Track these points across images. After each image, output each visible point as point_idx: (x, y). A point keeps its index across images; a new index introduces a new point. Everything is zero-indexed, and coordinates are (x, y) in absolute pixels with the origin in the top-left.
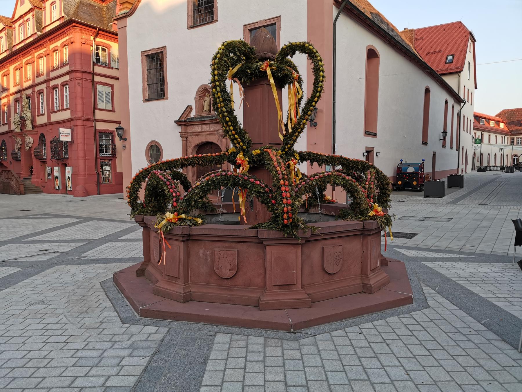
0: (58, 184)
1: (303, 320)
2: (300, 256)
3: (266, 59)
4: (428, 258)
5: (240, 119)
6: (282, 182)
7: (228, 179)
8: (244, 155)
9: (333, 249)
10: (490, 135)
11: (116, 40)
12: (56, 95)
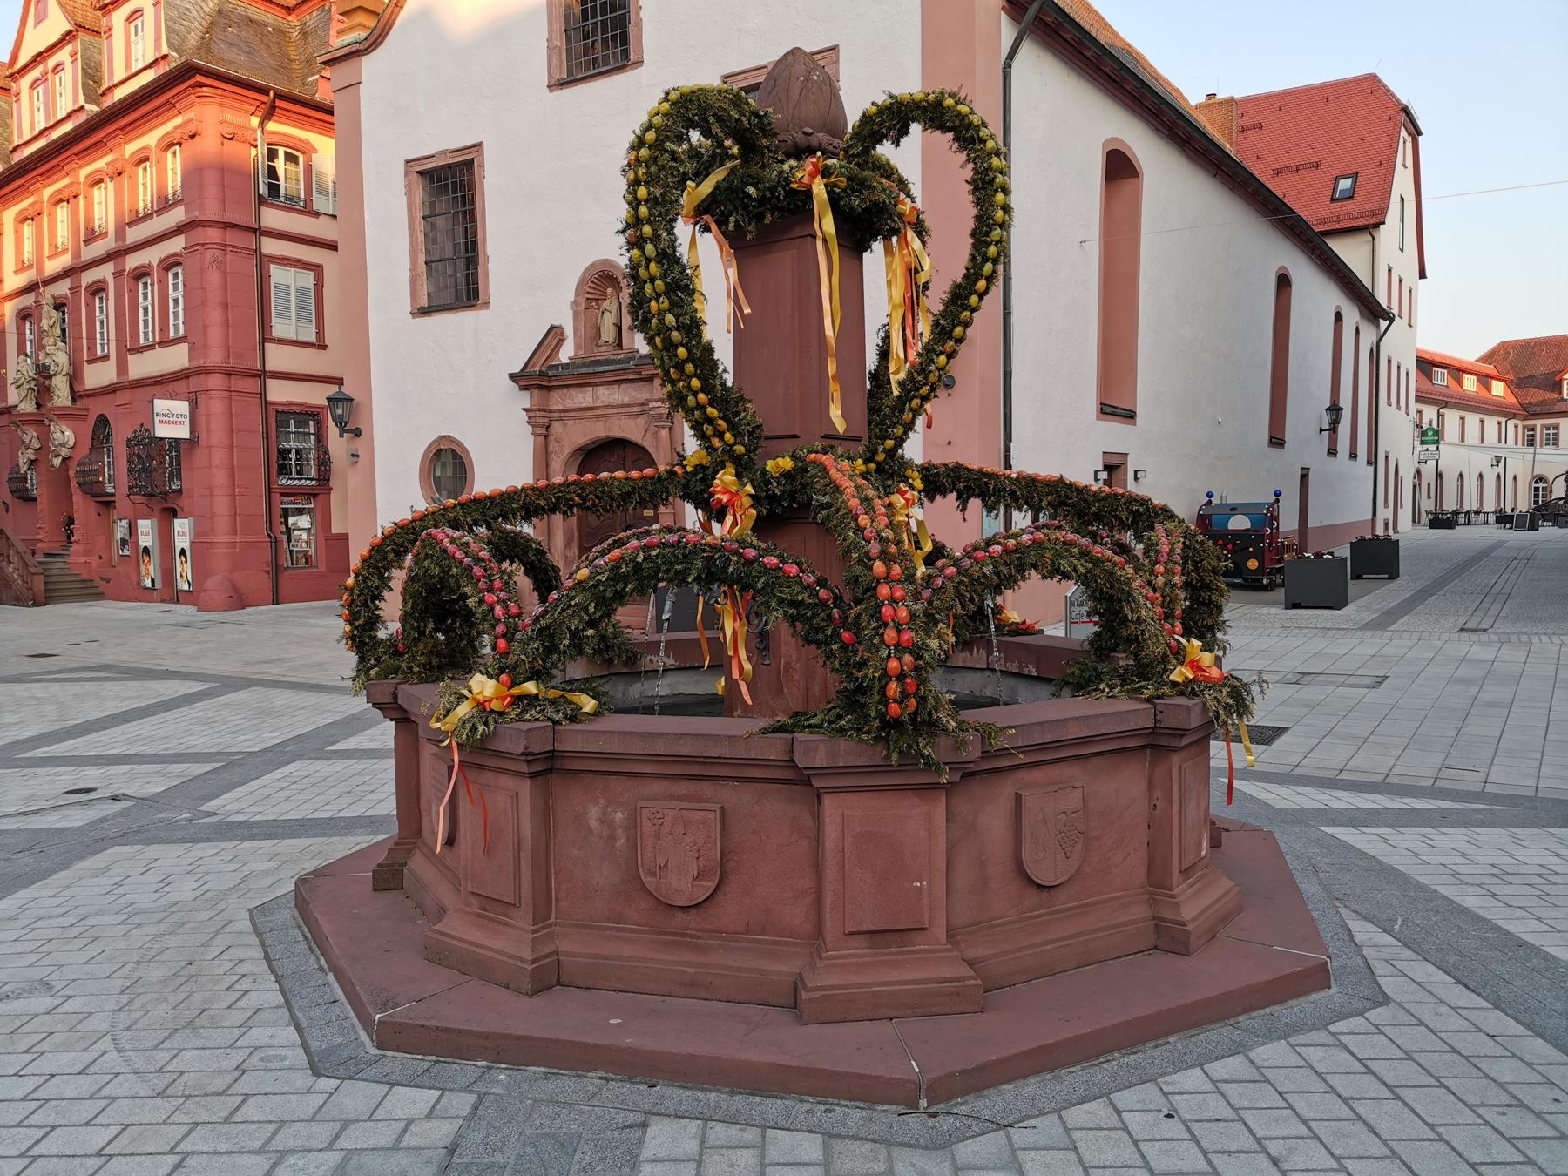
0: (150, 571)
1: (960, 1067)
2: (943, 825)
5: (724, 354)
6: (879, 567)
7: (687, 558)
8: (739, 476)
9: (1053, 798)
10: (1462, 419)
11: (327, 128)
12: (145, 298)
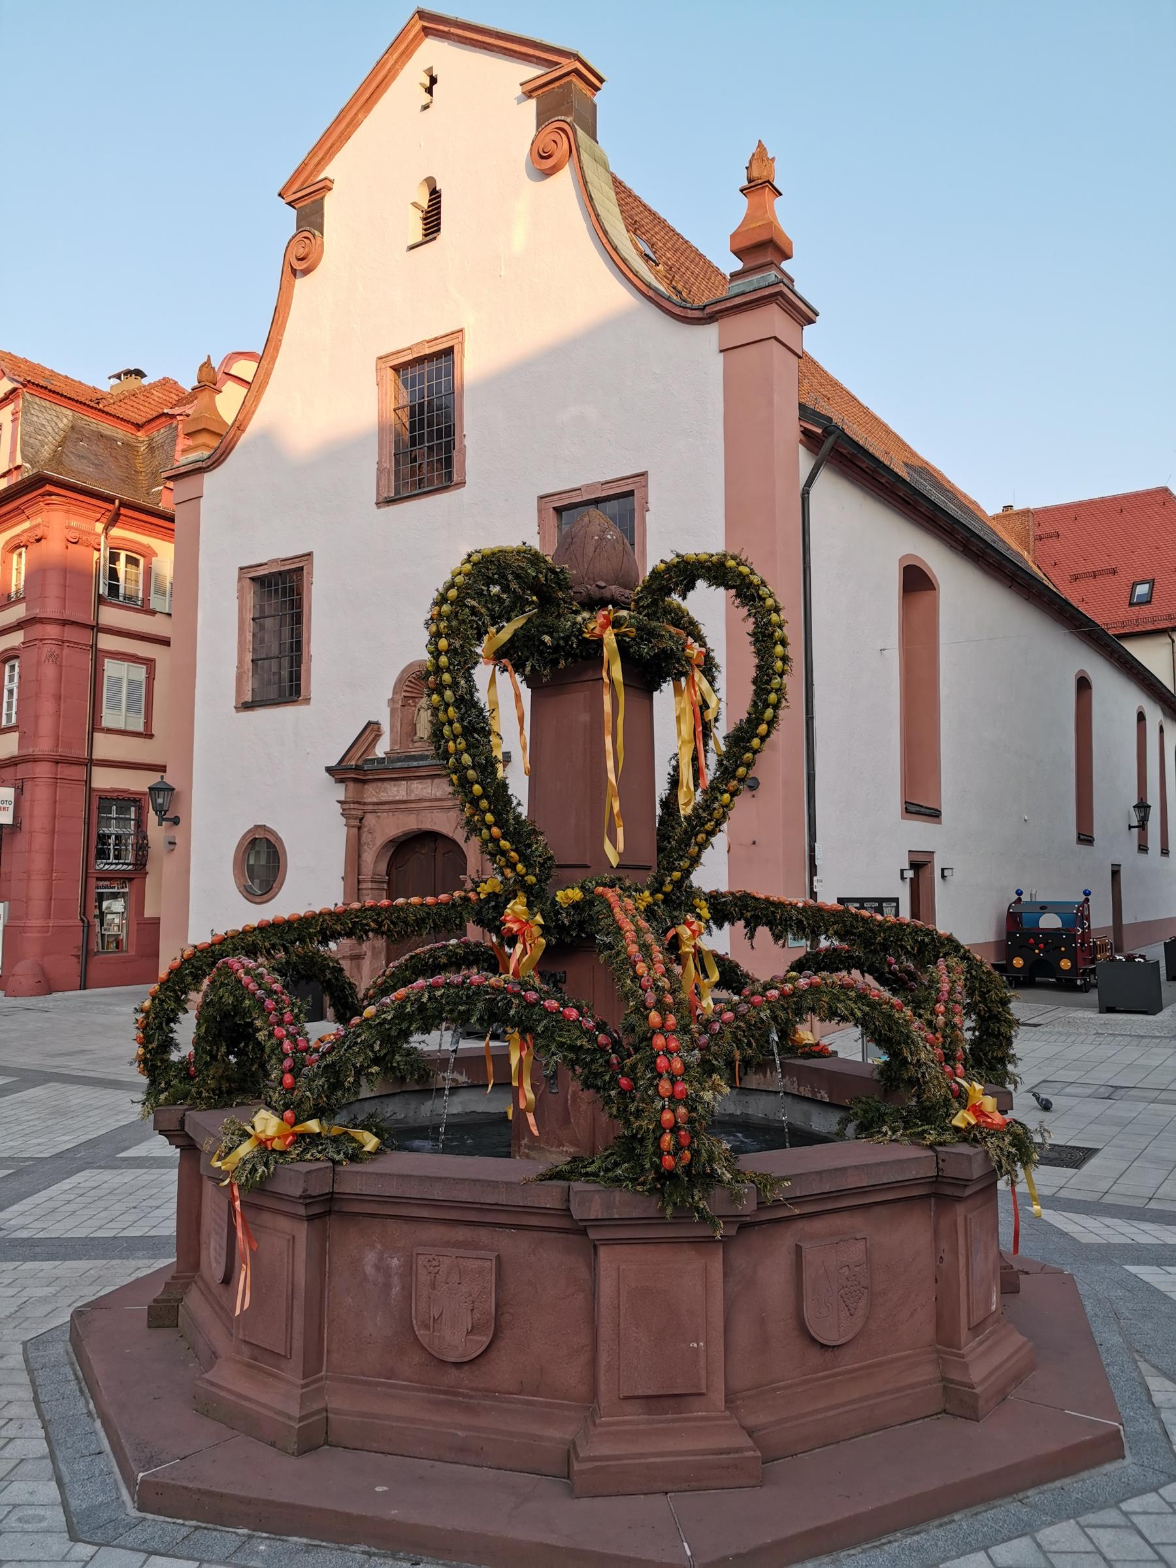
1: (734, 1551)
3: (602, 603)
4: (1145, 1247)
5: (518, 786)
8: (529, 905)
9: (835, 1250)
